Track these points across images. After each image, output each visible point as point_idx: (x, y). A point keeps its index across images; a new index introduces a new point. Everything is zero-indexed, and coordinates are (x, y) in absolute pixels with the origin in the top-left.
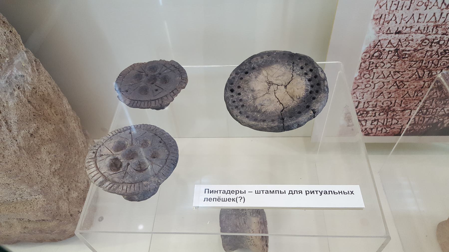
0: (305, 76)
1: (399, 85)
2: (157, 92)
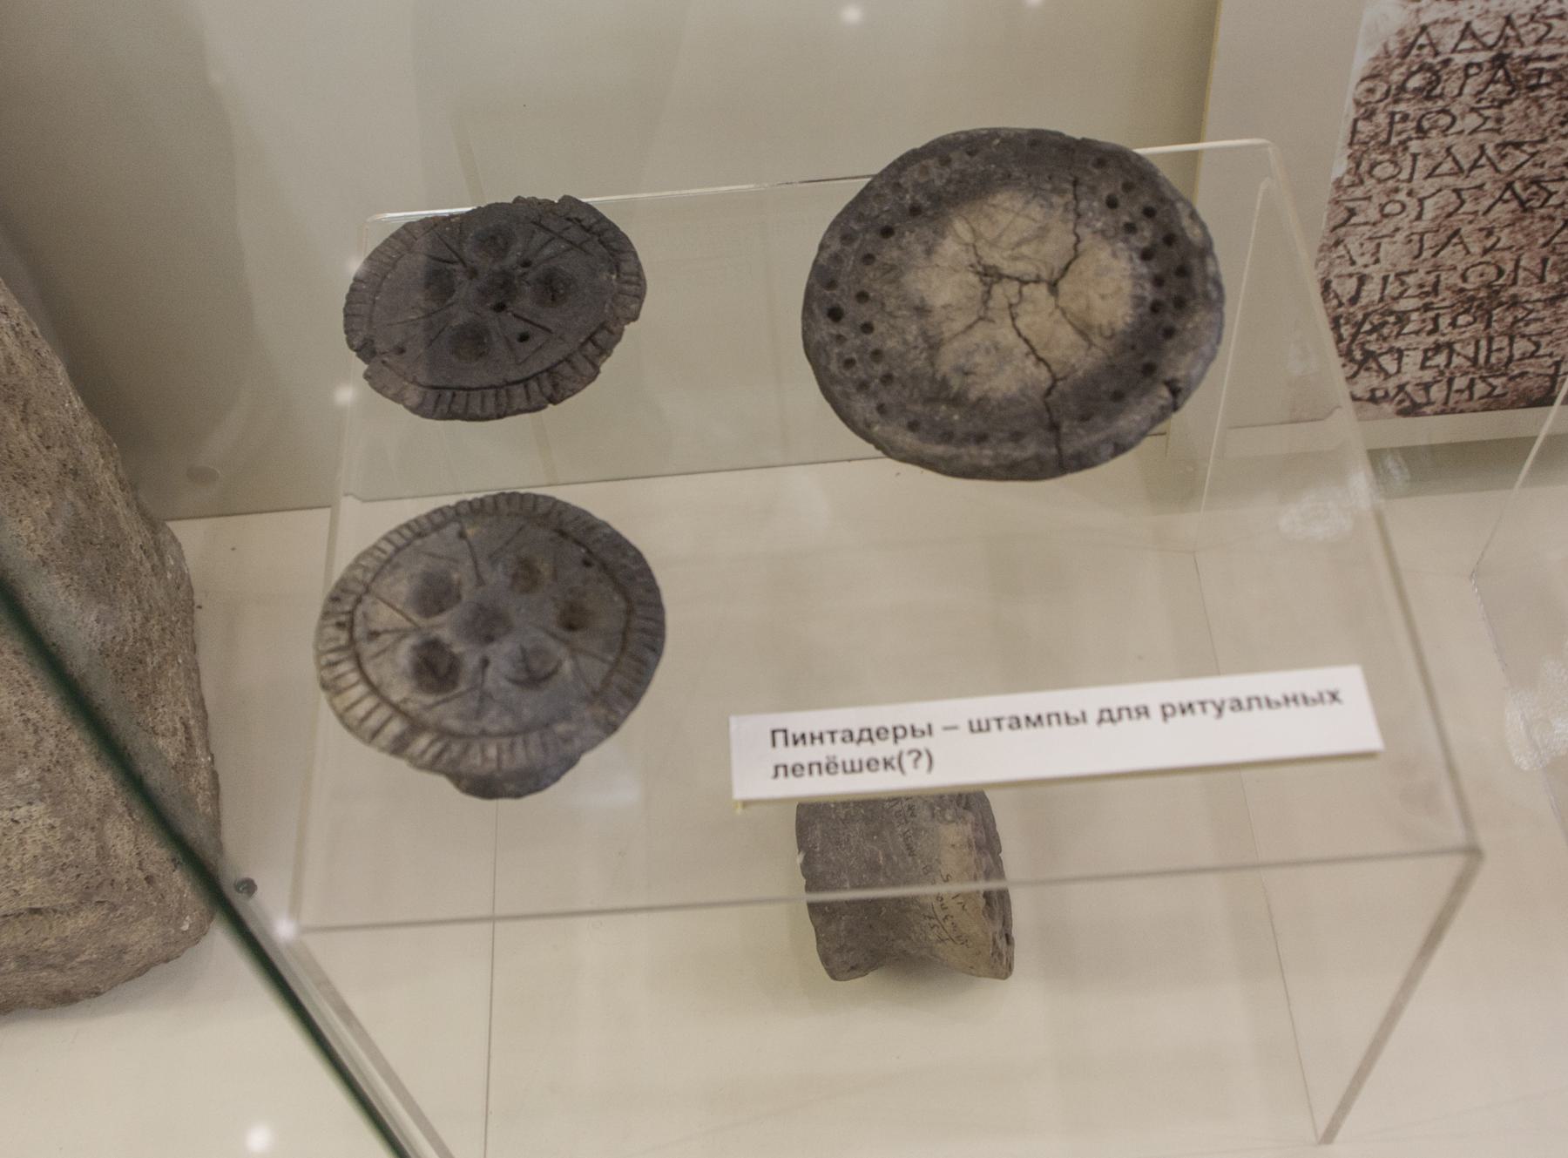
0: (1126, 241)
1: (1524, 196)
2: (528, 347)
